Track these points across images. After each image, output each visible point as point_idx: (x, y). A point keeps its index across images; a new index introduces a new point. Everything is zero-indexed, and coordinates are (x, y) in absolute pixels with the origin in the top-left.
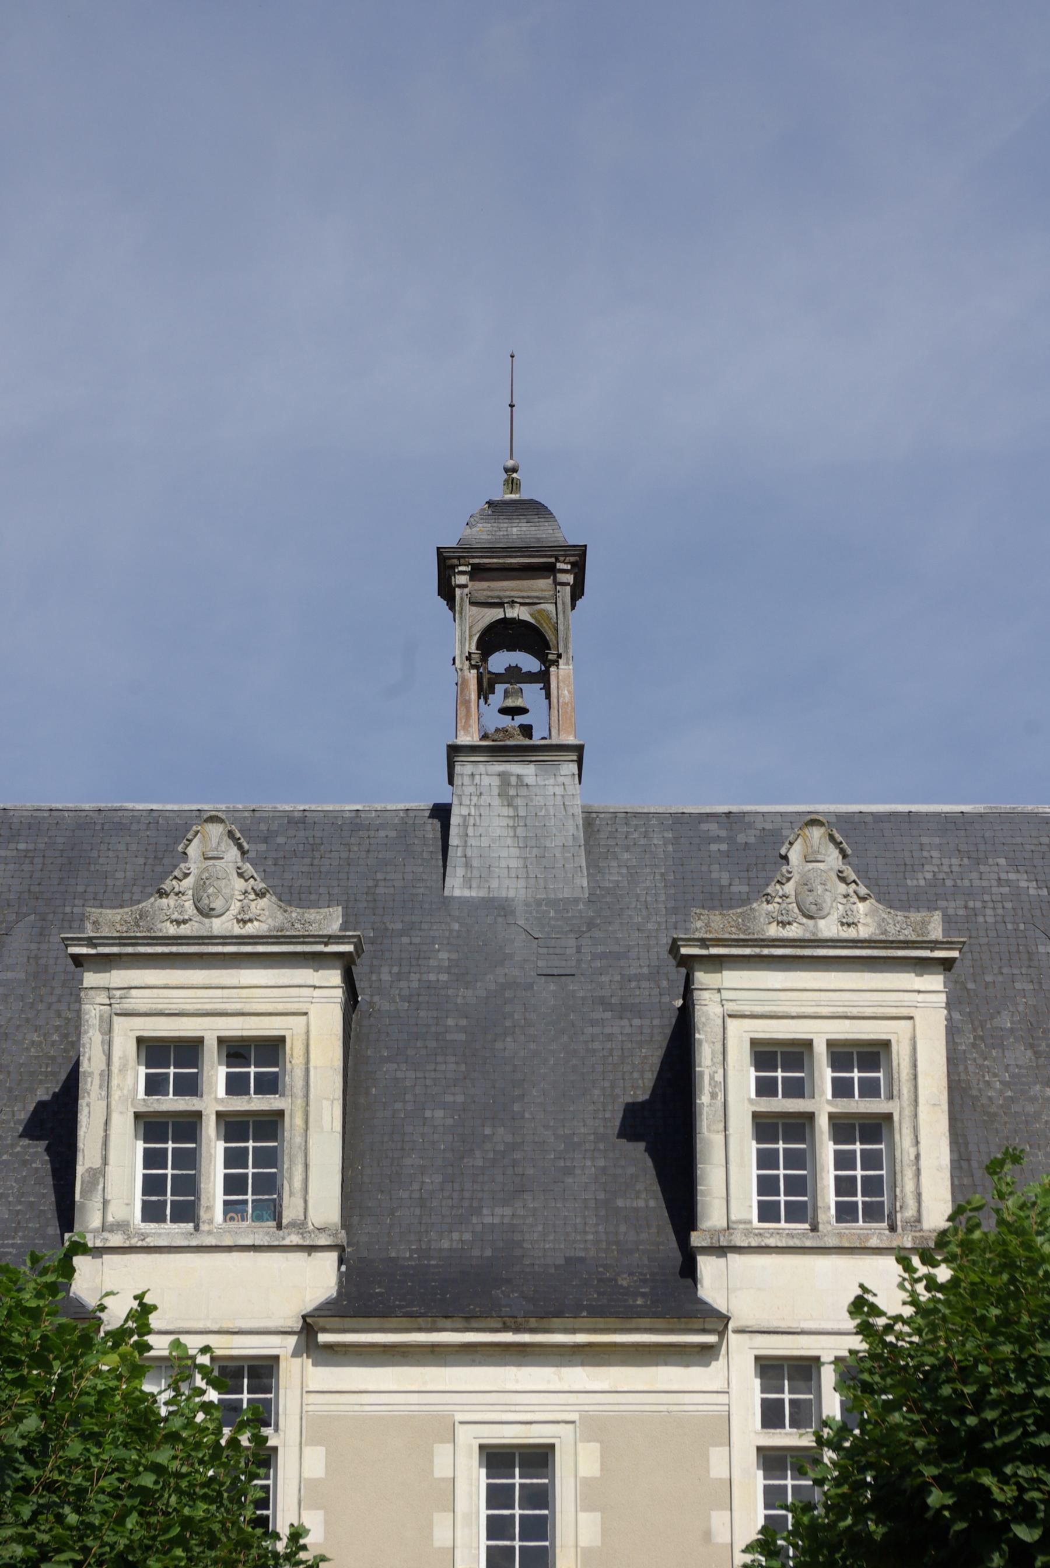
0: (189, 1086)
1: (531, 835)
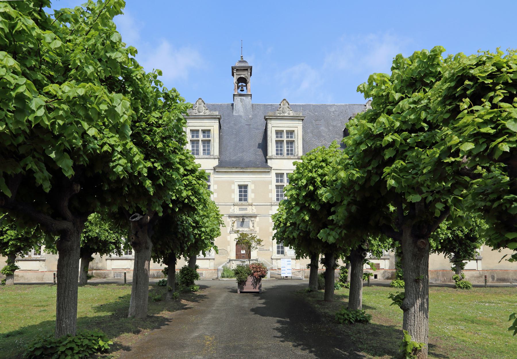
0: (197, 137)
1: (245, 107)
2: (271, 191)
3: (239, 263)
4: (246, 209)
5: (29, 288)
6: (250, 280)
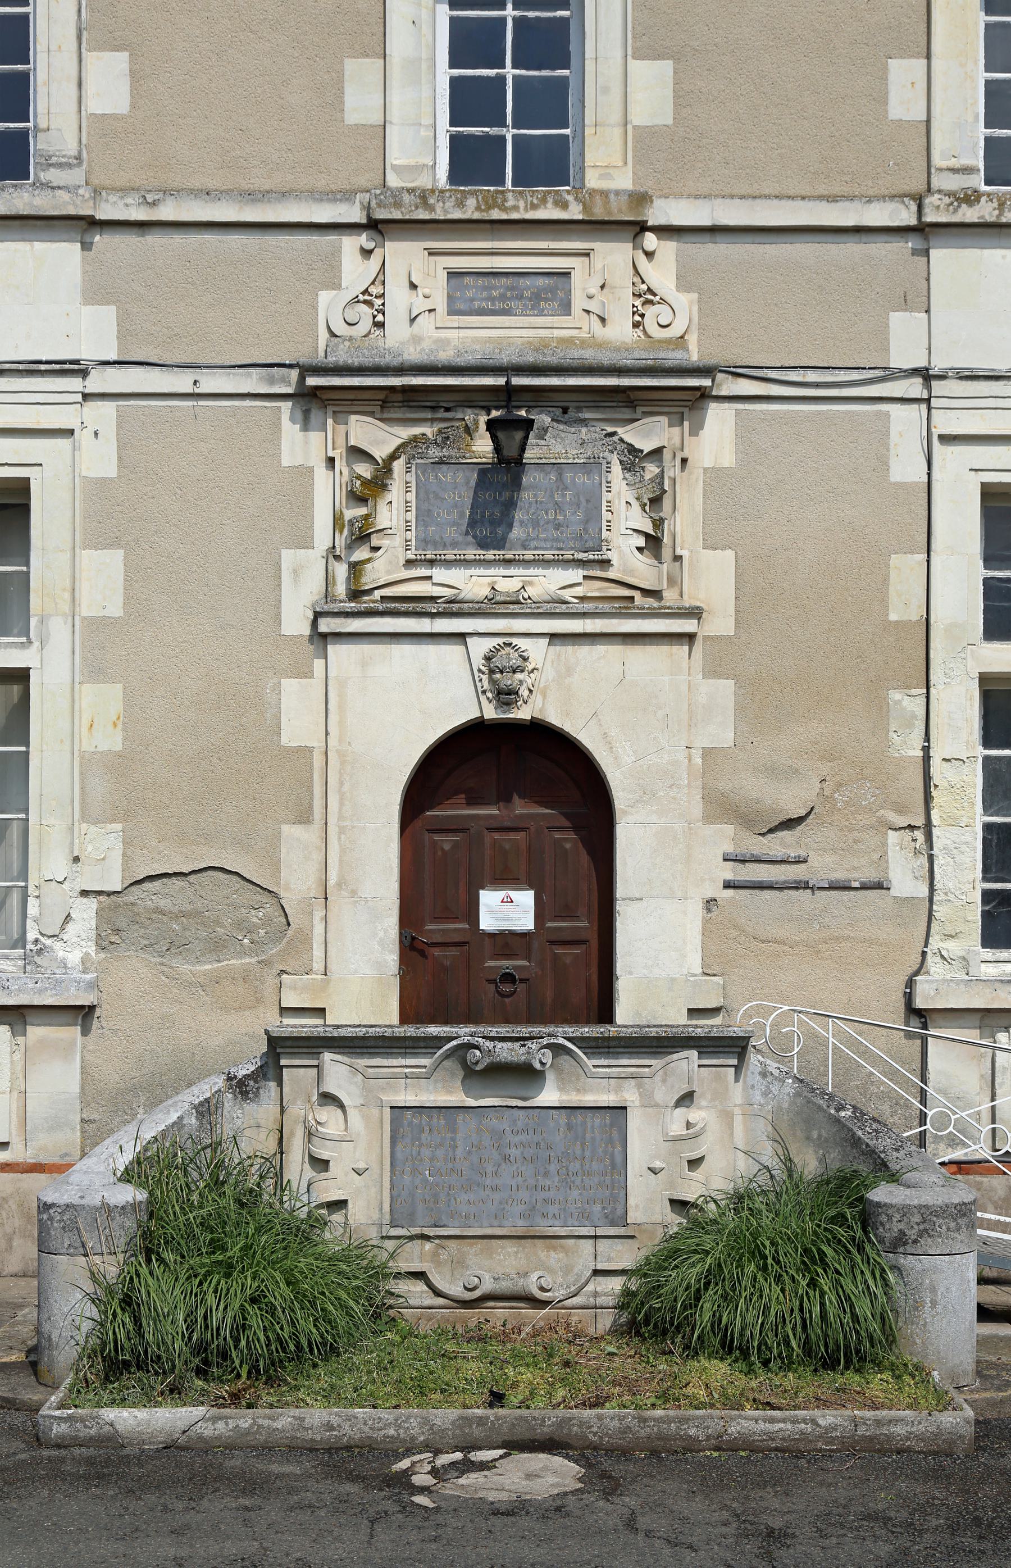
4: (552, 290)
5: (472, 1245)
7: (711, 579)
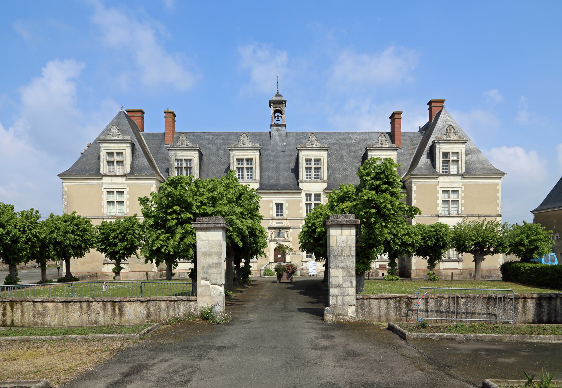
0: (242, 164)
1: (280, 135)
2: (301, 208)
3: (276, 264)
4: (282, 223)
6: (285, 275)
7: (291, 238)
